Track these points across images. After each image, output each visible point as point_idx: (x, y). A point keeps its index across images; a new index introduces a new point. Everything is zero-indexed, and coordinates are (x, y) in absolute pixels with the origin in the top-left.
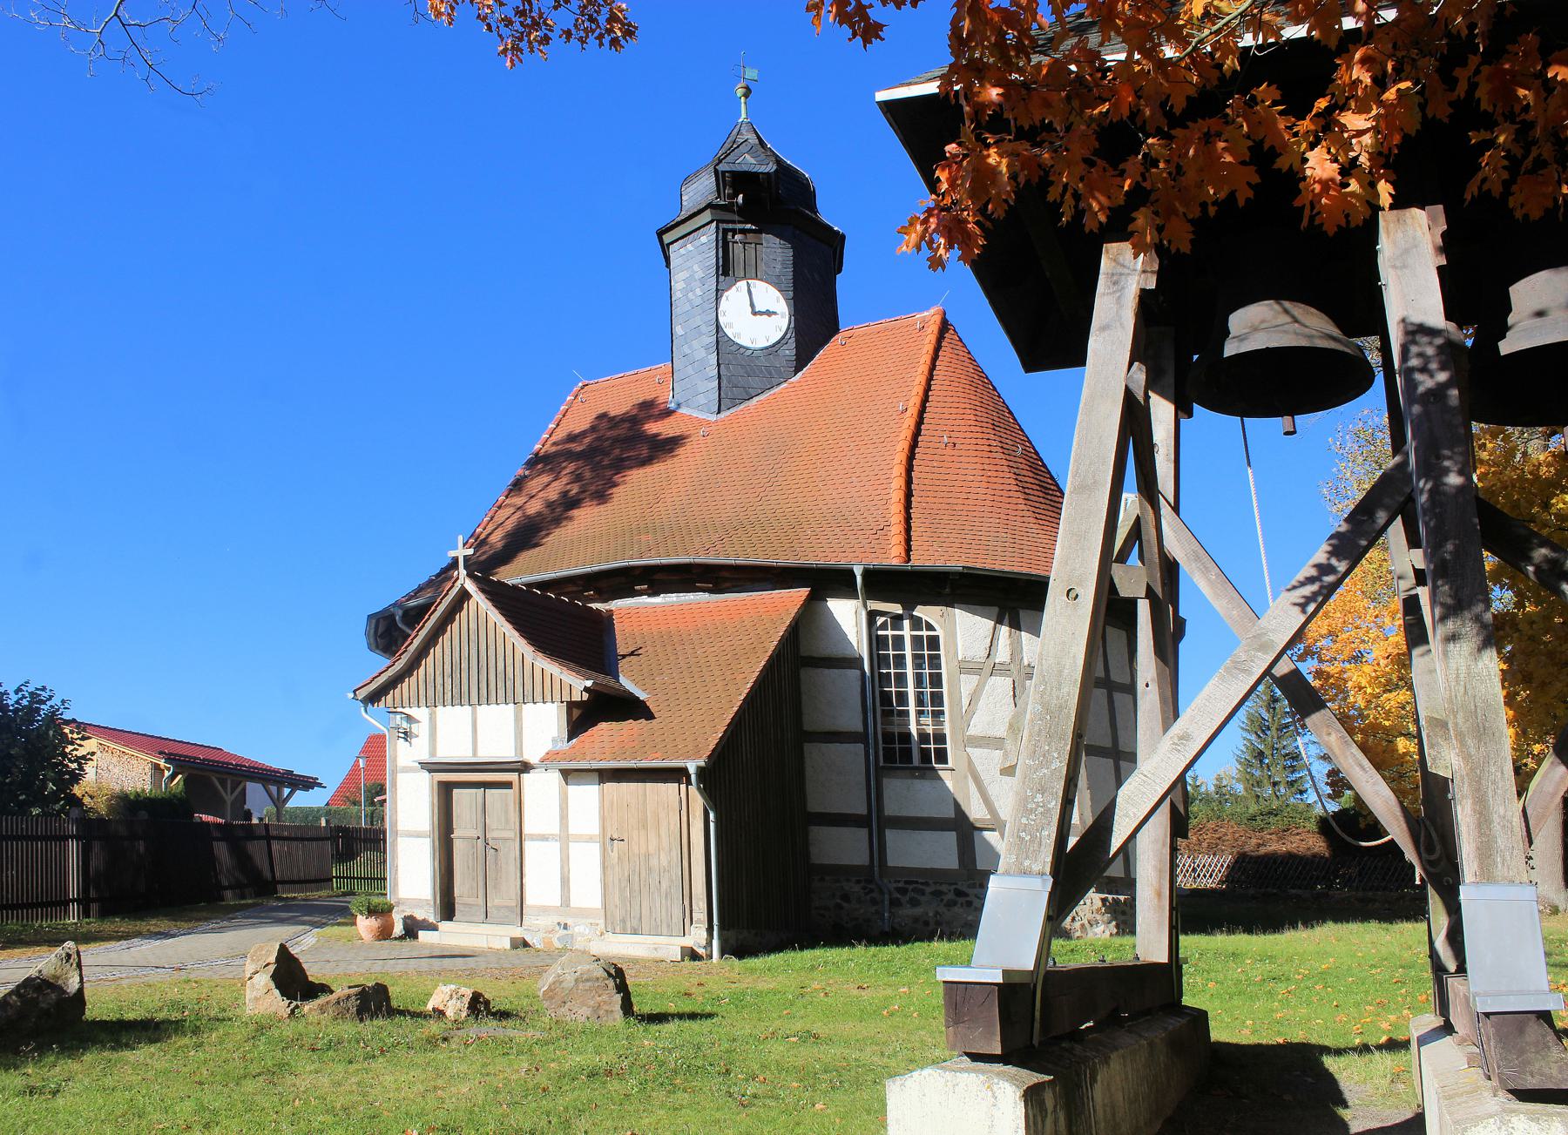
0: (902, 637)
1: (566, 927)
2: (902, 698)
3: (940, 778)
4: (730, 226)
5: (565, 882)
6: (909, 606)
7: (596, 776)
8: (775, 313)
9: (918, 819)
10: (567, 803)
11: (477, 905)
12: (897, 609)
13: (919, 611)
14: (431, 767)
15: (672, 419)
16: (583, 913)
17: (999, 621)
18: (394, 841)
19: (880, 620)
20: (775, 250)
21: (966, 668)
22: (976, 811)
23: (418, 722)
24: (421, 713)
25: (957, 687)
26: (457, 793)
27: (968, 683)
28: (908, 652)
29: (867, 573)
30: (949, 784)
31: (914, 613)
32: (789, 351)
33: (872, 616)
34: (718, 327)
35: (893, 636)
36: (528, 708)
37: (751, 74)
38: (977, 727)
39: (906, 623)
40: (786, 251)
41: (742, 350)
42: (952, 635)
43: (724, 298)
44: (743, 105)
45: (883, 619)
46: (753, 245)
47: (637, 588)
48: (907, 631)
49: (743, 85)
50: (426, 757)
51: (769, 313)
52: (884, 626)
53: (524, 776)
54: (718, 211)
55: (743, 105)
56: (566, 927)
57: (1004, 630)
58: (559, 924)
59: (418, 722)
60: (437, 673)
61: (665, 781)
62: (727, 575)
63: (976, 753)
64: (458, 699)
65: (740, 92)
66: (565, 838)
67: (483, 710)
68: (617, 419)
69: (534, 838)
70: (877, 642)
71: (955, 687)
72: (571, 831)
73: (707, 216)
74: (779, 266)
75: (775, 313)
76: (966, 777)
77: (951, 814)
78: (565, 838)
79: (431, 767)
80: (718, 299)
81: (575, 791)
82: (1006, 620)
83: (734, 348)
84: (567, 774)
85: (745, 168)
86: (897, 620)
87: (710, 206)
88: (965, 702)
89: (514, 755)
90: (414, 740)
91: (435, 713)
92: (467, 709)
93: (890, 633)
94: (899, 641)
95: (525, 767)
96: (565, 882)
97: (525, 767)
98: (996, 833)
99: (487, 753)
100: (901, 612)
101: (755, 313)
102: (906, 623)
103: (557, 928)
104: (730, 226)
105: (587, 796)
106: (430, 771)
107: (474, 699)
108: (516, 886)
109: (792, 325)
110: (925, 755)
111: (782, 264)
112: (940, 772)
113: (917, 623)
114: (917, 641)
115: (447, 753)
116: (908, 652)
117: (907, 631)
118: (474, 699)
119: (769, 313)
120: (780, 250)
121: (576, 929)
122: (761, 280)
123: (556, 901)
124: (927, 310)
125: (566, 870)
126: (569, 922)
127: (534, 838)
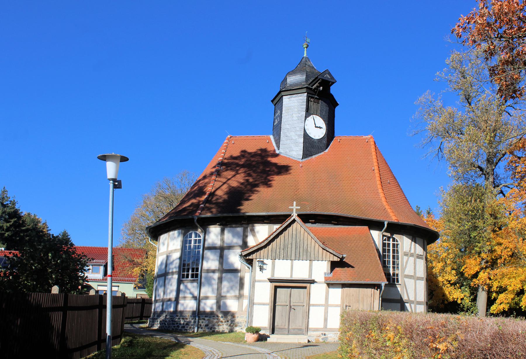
0: (390, 243)
1: (325, 335)
2: (389, 262)
3: (396, 287)
4: (311, 95)
5: (326, 320)
6: (392, 234)
7: (341, 286)
8: (322, 128)
9: (391, 299)
10: (329, 294)
11: (285, 329)
12: (389, 235)
13: (395, 236)
14: (271, 281)
15: (278, 157)
16: (332, 330)
17: (412, 241)
18: (252, 306)
19: (385, 238)
20: (321, 105)
21: (406, 254)
22: (405, 298)
23: (267, 264)
24: (268, 262)
25: (402, 260)
26: (278, 290)
27: (405, 258)
28: (391, 248)
29: (389, 224)
30: (399, 289)
31: (393, 236)
32: (325, 142)
33: (383, 236)
34: (304, 129)
35: (387, 243)
36: (315, 263)
37: (308, 40)
38: (406, 273)
39: (391, 239)
40: (327, 107)
41: (311, 139)
42: (403, 243)
43: (307, 120)
44: (305, 51)
45: (385, 238)
46: (316, 103)
47: (310, 221)
48: (391, 242)
49: (307, 44)
50: (270, 277)
51: (320, 128)
52: (385, 240)
53: (312, 285)
54: (308, 90)
55: (305, 51)
56: (325, 335)
57: (413, 243)
58: (322, 334)
59: (267, 264)
60: (277, 248)
61: (367, 288)
62: (341, 219)
63: (406, 280)
64: (286, 258)
65: (305, 46)
66: (326, 305)
67: (296, 262)
68: (253, 154)
69: (314, 305)
70: (384, 245)
71: (402, 259)
72: (329, 303)
73: (305, 90)
74: (324, 112)
75: (322, 128)
76: (404, 287)
77: (400, 298)
78: (326, 305)
79: (271, 281)
80: (305, 120)
81: (331, 290)
82: (414, 241)
83: (308, 138)
84: (330, 285)
85: (326, 79)
86: (389, 238)
87: (307, 87)
88: (405, 264)
89: (308, 277)
90: (263, 271)
91: (275, 262)
92: (289, 261)
93: (387, 242)
94: (389, 244)
95: (313, 282)
96: (326, 320)
97: (313, 282)
98: (409, 304)
99: (296, 277)
100: (390, 236)
101: (316, 127)
102: (391, 239)
103: (321, 335)
104: (311, 95)
105: (337, 293)
106: (271, 282)
107: (293, 258)
108: (306, 322)
109: (327, 133)
110: (394, 279)
111: (325, 112)
112: (397, 285)
113: (394, 240)
114: (394, 245)
115: (278, 275)
116: (391, 248)
117: (391, 242)
118: (293, 258)
119: (320, 128)
120: (325, 107)
121: (329, 336)
122: (318, 116)
123: (321, 326)
124: (368, 135)
125: (326, 316)
126: (326, 333)
127: (314, 305)
